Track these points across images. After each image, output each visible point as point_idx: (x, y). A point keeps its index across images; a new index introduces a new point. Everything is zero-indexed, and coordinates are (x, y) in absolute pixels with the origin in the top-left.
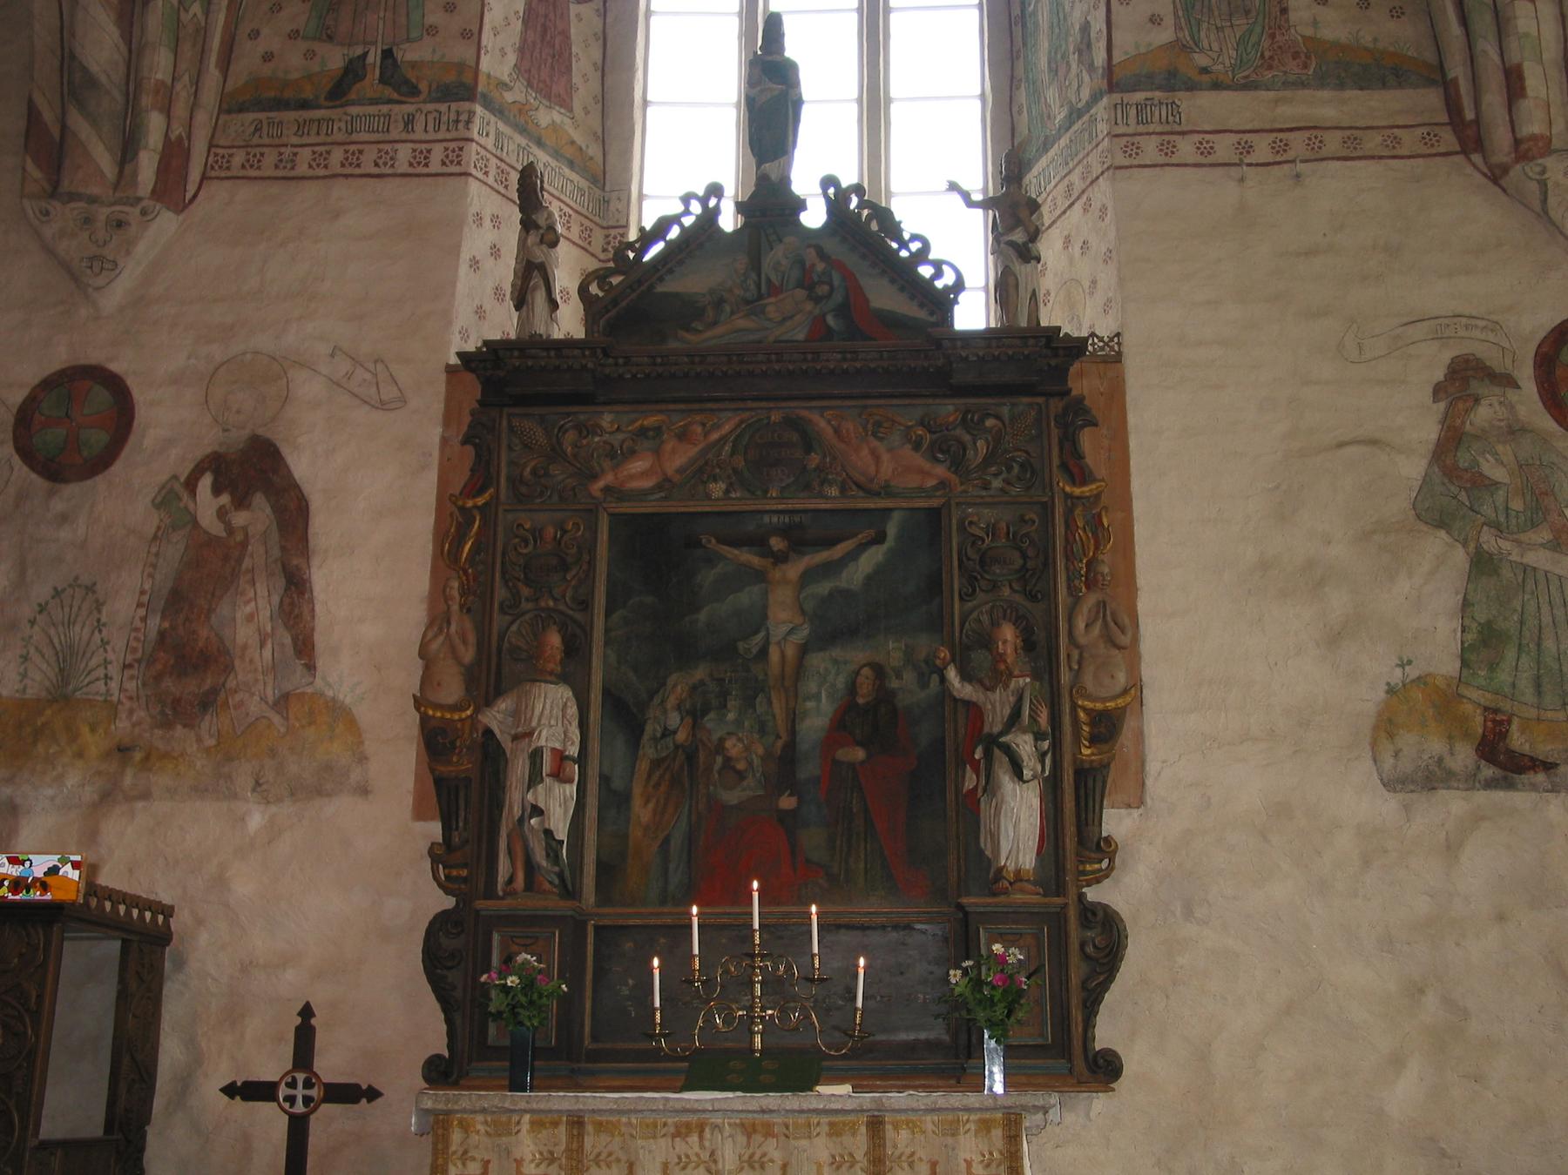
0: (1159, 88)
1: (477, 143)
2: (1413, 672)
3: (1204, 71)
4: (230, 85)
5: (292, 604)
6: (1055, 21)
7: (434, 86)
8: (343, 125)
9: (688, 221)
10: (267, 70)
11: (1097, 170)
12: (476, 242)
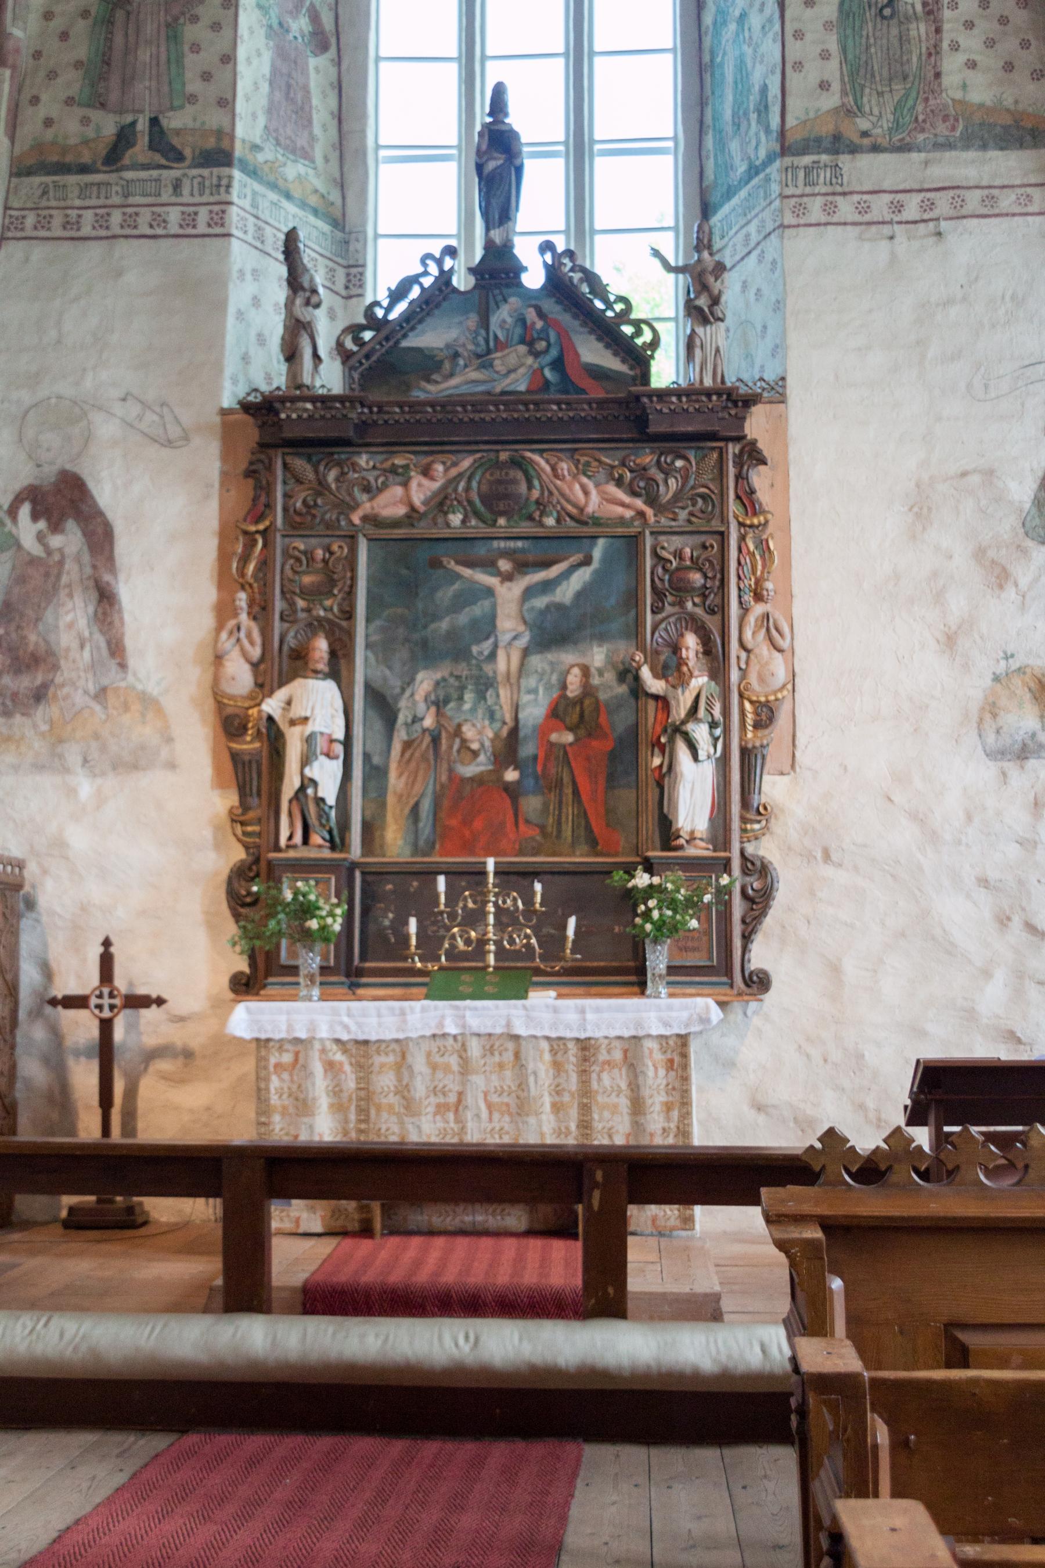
0: (826, 151)
1: (238, 206)
2: (1014, 664)
3: (865, 134)
4: (17, 151)
5: (105, 614)
6: (739, 77)
7: (197, 152)
8: (119, 189)
9: (427, 282)
10: (49, 135)
11: (770, 226)
12: (239, 295)
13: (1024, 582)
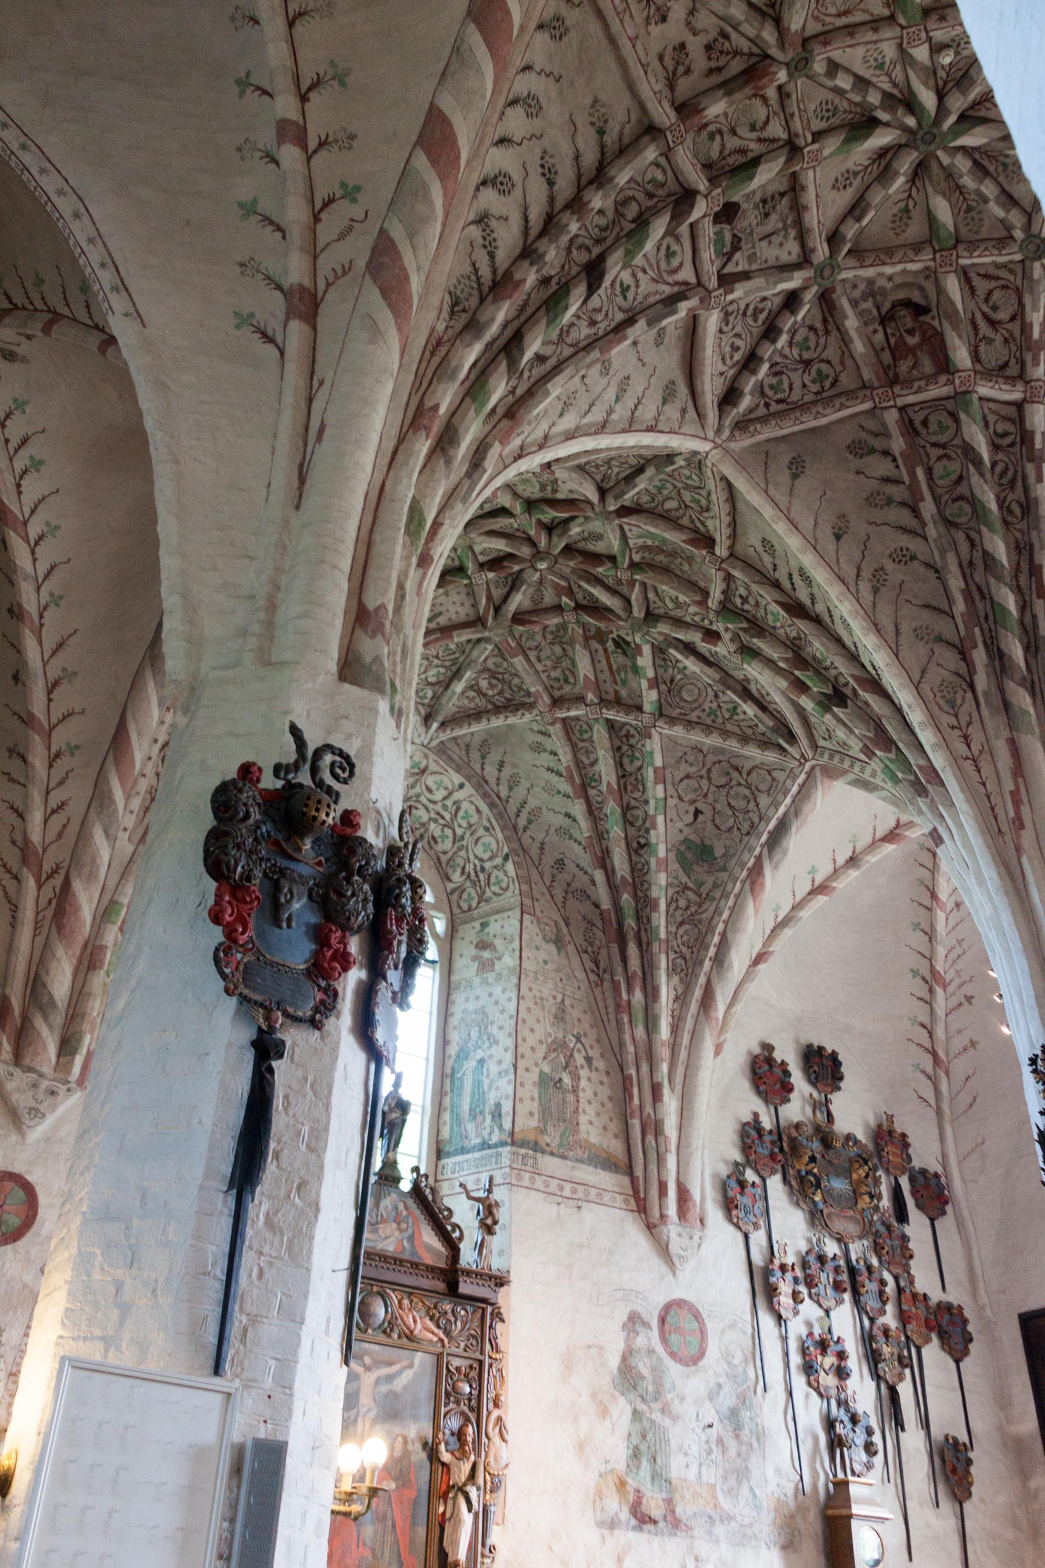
2: (609, 1467)
3: (548, 1145)
13: (615, 1416)
